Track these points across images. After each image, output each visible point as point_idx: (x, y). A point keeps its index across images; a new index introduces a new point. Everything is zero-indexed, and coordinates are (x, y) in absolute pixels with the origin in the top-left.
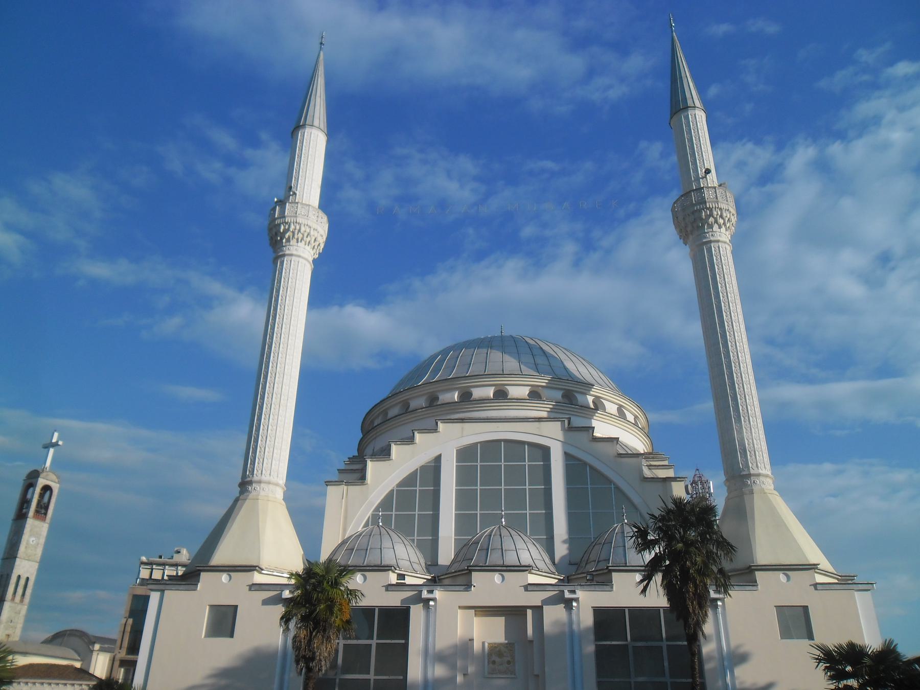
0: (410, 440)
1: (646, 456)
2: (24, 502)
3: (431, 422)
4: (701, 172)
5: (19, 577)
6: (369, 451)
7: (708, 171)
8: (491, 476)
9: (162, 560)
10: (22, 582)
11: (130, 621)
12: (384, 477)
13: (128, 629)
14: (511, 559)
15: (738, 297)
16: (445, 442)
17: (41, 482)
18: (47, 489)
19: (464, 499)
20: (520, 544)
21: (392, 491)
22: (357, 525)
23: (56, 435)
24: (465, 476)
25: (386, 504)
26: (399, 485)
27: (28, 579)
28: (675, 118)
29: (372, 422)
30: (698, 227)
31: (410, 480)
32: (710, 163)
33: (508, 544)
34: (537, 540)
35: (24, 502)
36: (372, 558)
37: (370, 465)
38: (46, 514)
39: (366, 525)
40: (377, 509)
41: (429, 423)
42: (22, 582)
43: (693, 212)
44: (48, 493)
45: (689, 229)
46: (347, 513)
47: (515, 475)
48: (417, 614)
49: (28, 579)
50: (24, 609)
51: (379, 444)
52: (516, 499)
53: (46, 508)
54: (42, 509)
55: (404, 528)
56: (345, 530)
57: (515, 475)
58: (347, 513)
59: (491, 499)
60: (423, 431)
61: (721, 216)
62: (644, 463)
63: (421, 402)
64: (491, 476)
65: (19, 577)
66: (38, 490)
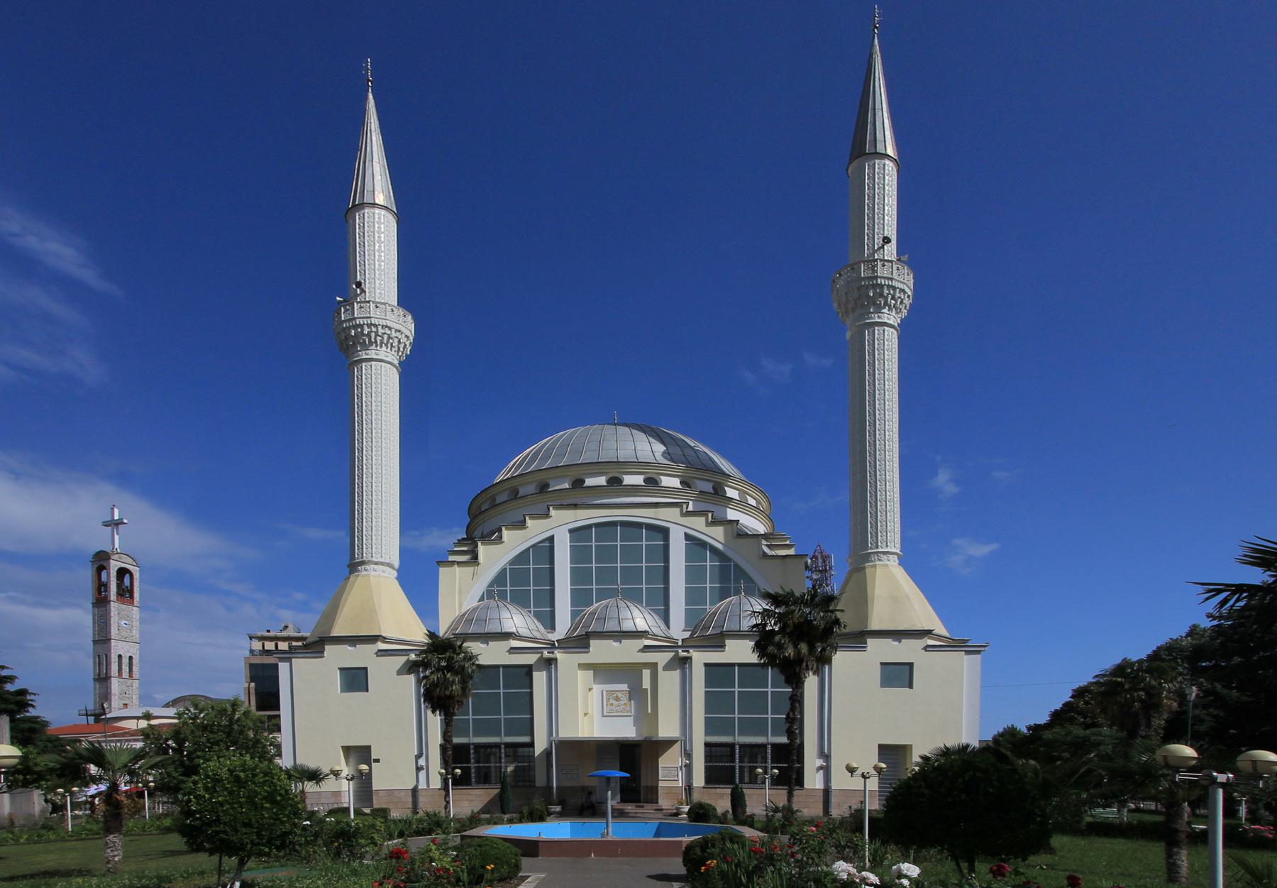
0: (521, 525)
1: (765, 536)
2: (101, 587)
3: (543, 507)
4: (878, 242)
5: (120, 656)
6: (477, 533)
7: (887, 240)
8: (606, 554)
9: (272, 634)
10: (125, 661)
11: (253, 685)
12: (494, 557)
13: (253, 691)
14: (627, 626)
15: (896, 406)
16: (559, 525)
17: (114, 565)
18: (122, 572)
19: (579, 576)
20: (636, 612)
21: (504, 570)
22: (470, 602)
23: (116, 511)
24: (579, 555)
25: (500, 579)
26: (512, 562)
27: (131, 658)
28: (855, 163)
29: (480, 506)
30: (863, 305)
31: (522, 558)
32: (891, 231)
33: (625, 614)
34: (654, 611)
35: (101, 587)
36: (492, 627)
37: (482, 549)
38: (132, 597)
39: (482, 599)
40: (491, 585)
41: (541, 508)
42: (125, 661)
43: (860, 288)
44: (127, 576)
45: (850, 306)
46: (460, 592)
47: (631, 553)
48: (539, 678)
49: (131, 658)
50: (136, 684)
51: (488, 527)
52: (631, 575)
53: (131, 592)
54: (126, 593)
55: (520, 600)
56: (460, 605)
57: (631, 553)
58: (460, 592)
59: (606, 575)
60: (533, 517)
61: (893, 298)
62: (764, 542)
63: (531, 489)
64: (606, 554)
65: (120, 656)
66: (113, 573)
